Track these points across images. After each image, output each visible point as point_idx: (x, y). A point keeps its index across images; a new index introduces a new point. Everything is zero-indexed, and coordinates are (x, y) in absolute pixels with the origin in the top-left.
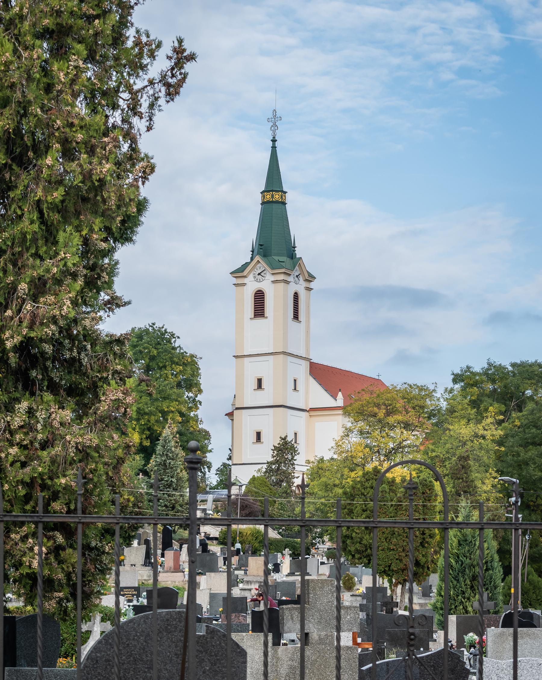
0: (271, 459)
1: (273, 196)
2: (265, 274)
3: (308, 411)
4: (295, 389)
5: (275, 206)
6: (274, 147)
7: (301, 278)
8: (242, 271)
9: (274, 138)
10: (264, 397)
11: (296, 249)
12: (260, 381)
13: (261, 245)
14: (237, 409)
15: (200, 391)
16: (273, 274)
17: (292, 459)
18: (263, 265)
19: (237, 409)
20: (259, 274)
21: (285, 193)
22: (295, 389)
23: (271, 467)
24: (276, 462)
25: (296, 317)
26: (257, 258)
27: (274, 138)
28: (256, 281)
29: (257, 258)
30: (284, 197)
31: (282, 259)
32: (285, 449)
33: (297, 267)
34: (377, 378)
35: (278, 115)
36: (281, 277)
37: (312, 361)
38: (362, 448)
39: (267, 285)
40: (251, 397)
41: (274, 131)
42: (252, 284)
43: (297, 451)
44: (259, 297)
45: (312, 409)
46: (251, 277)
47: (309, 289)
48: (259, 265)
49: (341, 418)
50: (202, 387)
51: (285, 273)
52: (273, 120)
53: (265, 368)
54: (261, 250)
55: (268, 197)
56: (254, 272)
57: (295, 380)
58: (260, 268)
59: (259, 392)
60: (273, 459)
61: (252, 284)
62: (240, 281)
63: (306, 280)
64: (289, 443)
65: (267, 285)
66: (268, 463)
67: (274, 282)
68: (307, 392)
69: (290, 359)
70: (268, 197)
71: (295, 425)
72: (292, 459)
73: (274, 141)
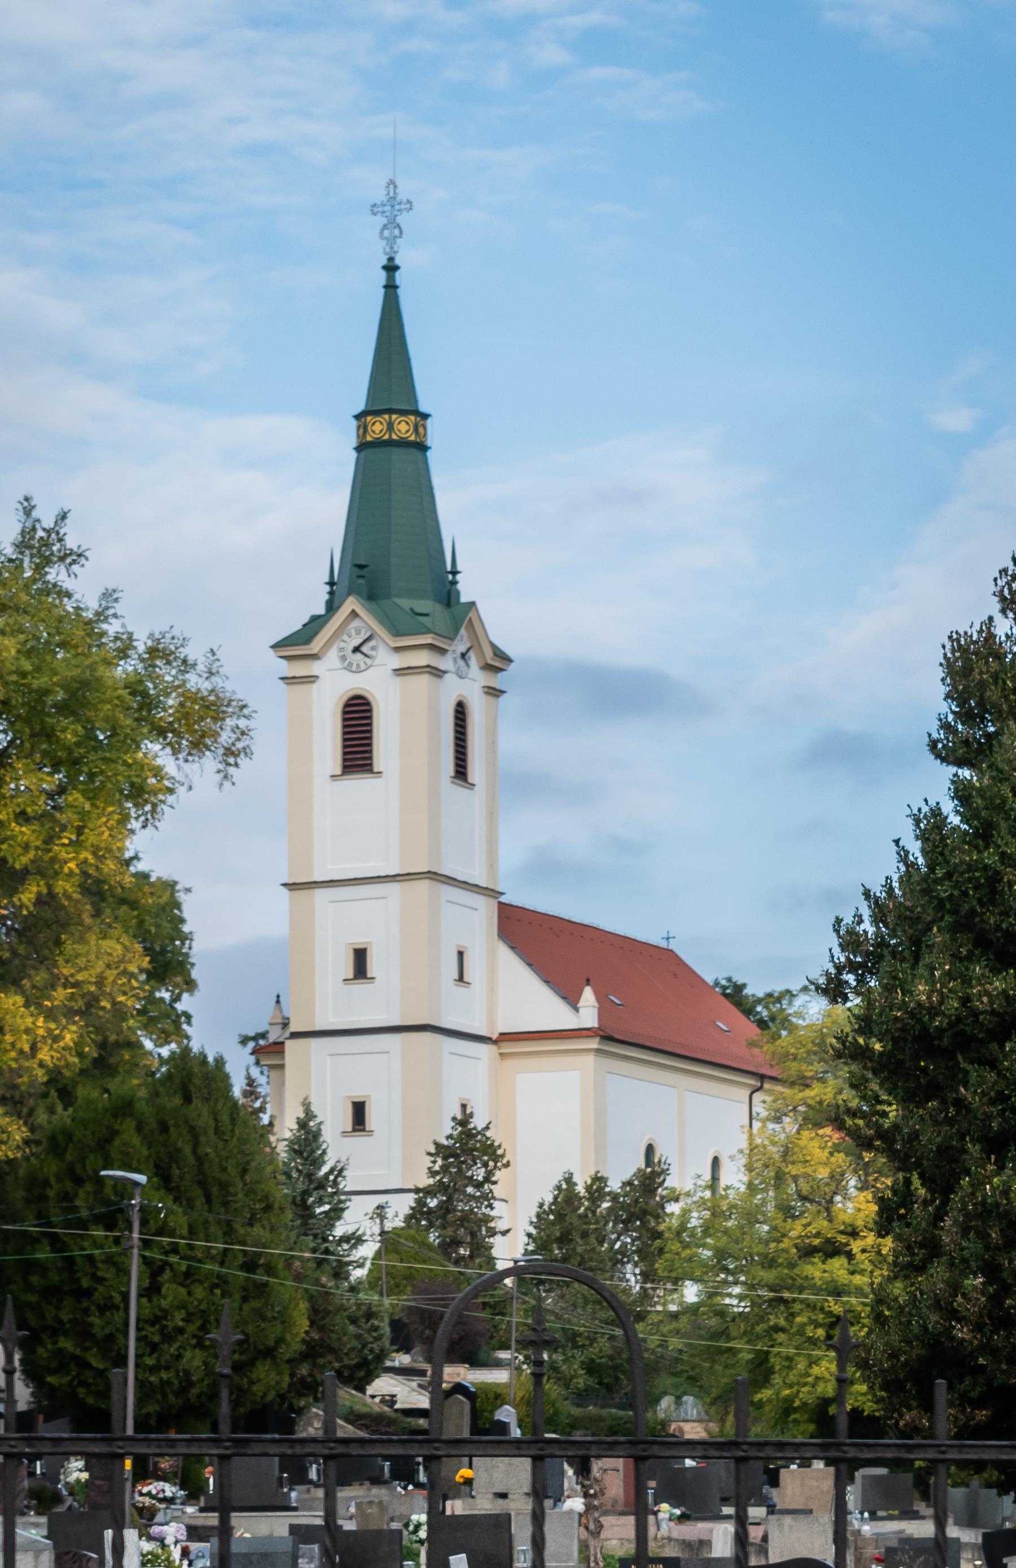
0: (425, 1181)
1: (390, 426)
2: (373, 648)
3: (495, 1042)
4: (461, 978)
5: (397, 454)
6: (391, 287)
7: (473, 661)
8: (308, 641)
9: (391, 259)
10: (369, 1005)
11: (458, 577)
12: (360, 956)
13: (361, 567)
14: (295, 1035)
15: (190, 985)
16: (398, 649)
17: (487, 1179)
18: (368, 621)
19: (295, 1035)
20: (357, 649)
21: (425, 416)
22: (461, 978)
23: (425, 1204)
24: (441, 1188)
25: (461, 772)
26: (351, 604)
27: (391, 259)
28: (349, 668)
29: (351, 604)
30: (421, 430)
31: (423, 605)
32: (467, 1154)
33: (463, 631)
34: (663, 944)
35: (402, 196)
36: (422, 658)
37: (503, 899)
38: (826, 1153)
39: (379, 679)
40: (332, 1002)
41: (391, 241)
42: (333, 682)
43: (502, 1156)
44: (357, 716)
45: (506, 1037)
46: (332, 657)
47: (494, 692)
48: (356, 623)
49: (590, 1059)
50: (195, 974)
51: (432, 647)
52: (388, 208)
53: (375, 919)
54: (361, 581)
55: (377, 428)
56: (342, 645)
57: (461, 954)
58: (358, 632)
59: (360, 988)
60: (431, 1181)
61: (333, 682)
62: (300, 669)
63: (488, 667)
64: (479, 1133)
65: (379, 679)
66: (417, 1191)
67: (400, 672)
68: (492, 988)
69: (449, 892)
70: (377, 427)
71: (469, 1080)
72: (487, 1179)
73: (391, 268)
